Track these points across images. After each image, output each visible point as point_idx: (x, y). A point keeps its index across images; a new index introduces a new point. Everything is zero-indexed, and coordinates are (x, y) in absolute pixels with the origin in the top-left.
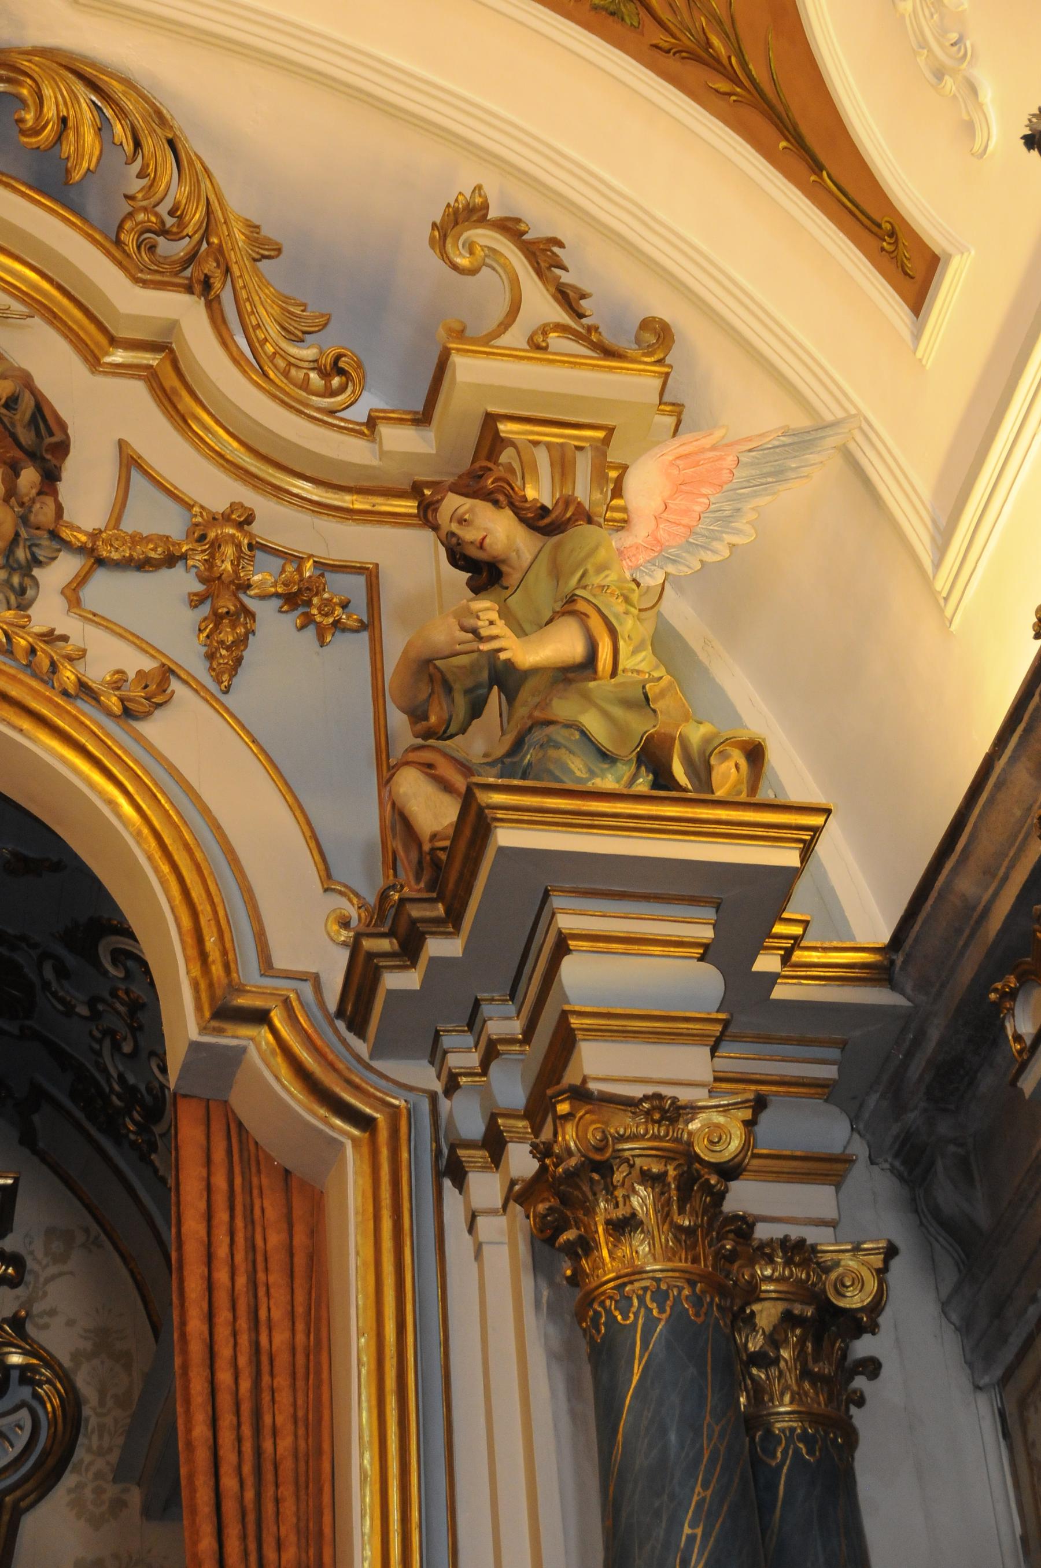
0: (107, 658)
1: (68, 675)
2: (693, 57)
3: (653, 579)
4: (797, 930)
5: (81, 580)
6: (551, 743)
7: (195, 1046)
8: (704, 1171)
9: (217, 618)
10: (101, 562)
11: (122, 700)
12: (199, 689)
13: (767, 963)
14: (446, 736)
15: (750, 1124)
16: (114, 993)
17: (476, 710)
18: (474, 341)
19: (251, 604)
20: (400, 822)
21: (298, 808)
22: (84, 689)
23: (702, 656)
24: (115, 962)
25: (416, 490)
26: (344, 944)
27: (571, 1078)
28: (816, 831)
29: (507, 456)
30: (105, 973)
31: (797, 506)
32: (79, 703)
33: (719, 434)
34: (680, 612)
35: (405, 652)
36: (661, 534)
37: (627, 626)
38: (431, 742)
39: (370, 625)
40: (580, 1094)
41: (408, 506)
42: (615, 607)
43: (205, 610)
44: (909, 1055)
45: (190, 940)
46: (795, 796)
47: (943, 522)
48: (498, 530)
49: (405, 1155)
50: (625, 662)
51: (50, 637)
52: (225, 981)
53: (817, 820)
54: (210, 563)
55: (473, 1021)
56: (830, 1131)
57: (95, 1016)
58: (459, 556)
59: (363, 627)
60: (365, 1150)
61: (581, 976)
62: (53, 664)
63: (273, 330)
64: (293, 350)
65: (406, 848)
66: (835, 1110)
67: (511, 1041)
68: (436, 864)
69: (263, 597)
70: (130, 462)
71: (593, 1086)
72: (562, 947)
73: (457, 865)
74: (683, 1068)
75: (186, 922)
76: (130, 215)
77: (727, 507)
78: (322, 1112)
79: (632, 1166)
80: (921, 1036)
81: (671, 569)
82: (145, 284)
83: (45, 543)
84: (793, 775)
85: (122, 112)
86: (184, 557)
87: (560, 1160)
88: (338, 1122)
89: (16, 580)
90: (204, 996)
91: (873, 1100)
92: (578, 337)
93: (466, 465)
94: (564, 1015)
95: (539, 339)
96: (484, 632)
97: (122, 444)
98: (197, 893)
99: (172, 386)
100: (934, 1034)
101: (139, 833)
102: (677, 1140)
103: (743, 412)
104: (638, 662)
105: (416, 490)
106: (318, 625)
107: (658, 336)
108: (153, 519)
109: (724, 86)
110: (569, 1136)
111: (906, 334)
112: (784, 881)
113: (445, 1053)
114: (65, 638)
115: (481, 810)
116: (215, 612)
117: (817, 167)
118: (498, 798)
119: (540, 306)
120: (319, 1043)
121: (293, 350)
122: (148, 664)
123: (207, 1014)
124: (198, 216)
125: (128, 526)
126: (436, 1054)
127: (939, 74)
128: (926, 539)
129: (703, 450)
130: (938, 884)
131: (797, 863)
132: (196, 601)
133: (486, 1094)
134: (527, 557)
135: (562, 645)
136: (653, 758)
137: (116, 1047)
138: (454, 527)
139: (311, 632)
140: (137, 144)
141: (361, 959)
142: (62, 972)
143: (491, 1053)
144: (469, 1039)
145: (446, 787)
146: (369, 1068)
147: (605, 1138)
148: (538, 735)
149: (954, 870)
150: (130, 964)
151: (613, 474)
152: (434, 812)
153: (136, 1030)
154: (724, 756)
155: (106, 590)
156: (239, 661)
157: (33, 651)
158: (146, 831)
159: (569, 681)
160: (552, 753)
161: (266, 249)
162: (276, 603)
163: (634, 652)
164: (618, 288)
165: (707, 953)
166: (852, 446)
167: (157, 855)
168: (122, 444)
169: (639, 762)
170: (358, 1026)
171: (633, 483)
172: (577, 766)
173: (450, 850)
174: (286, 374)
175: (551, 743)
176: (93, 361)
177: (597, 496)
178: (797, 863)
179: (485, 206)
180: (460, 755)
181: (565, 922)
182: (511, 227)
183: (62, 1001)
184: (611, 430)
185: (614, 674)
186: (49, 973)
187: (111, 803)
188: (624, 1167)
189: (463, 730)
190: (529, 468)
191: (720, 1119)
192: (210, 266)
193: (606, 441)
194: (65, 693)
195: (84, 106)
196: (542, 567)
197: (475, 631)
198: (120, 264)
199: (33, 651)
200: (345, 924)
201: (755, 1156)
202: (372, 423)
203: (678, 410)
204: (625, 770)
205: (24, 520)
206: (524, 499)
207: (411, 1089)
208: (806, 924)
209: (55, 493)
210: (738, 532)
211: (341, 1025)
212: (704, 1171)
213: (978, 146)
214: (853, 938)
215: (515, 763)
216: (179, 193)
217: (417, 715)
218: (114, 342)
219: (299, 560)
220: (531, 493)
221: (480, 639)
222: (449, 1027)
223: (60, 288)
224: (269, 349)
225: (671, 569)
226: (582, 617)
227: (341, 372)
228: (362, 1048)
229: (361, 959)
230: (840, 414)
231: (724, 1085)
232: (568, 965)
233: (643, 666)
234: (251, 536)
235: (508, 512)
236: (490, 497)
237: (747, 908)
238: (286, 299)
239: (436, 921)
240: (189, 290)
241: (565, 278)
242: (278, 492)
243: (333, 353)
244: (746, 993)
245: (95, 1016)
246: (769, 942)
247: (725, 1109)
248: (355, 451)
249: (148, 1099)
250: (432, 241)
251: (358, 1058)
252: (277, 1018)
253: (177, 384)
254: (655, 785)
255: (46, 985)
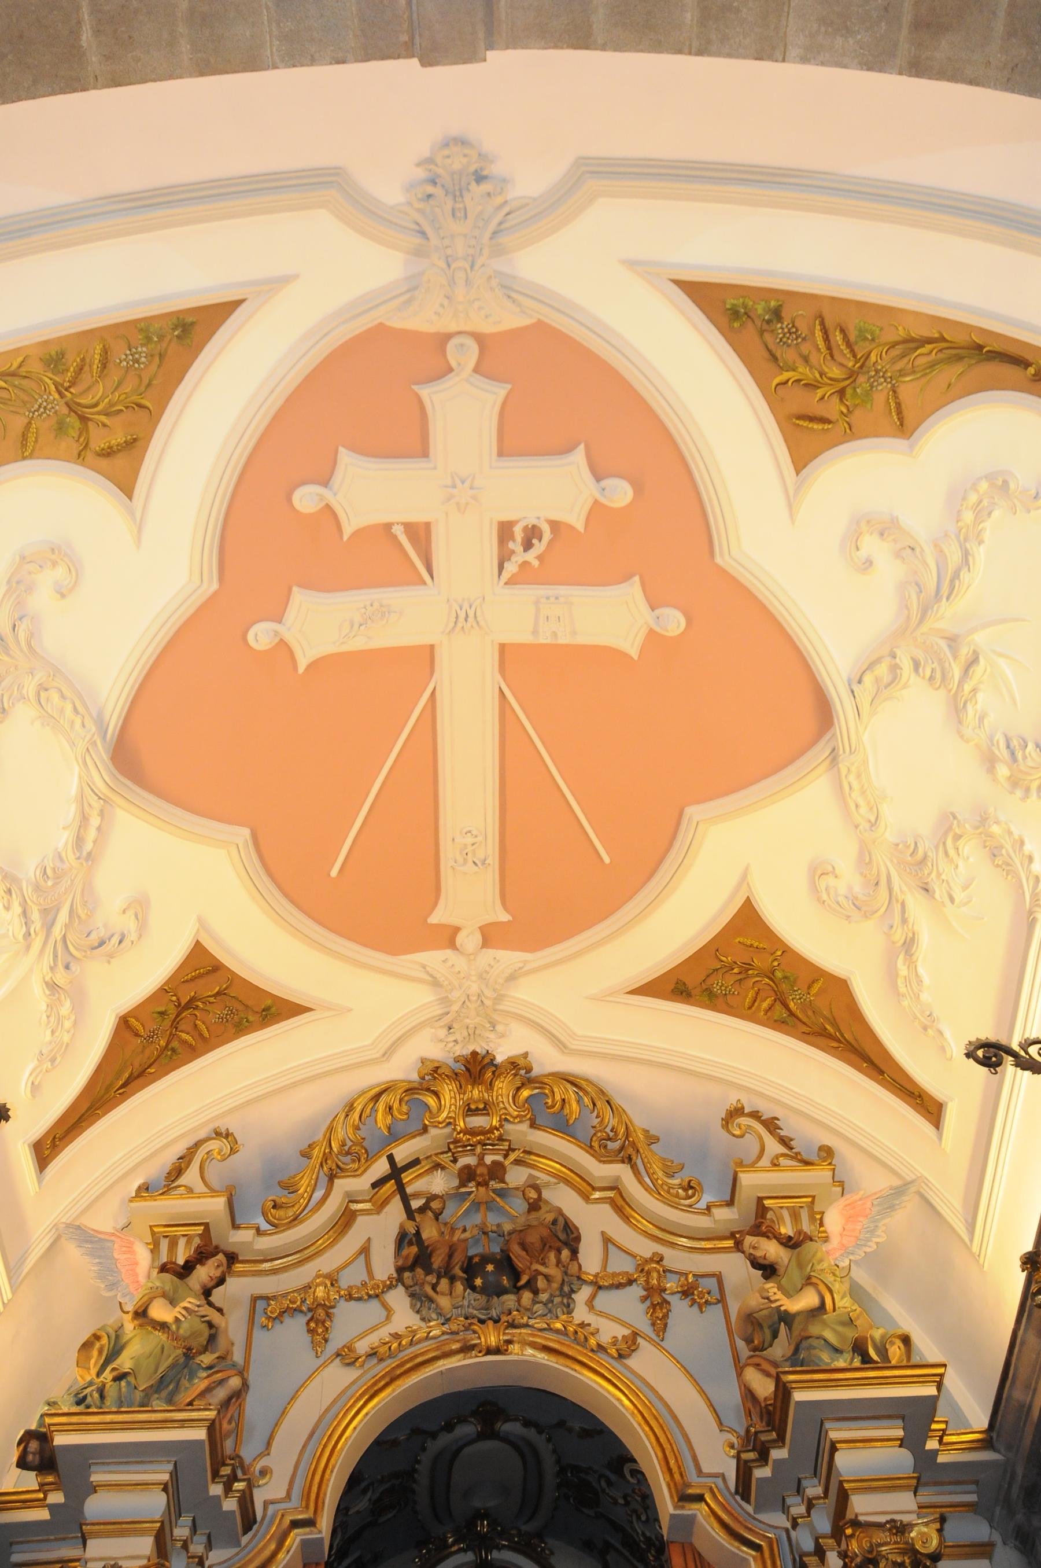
0: (609, 1332)
1: (592, 1342)
2: (820, 1035)
3: (845, 1263)
4: (943, 1426)
5: (593, 1297)
6: (811, 1347)
7: (672, 1516)
8: (923, 1559)
9: (654, 1306)
10: (600, 1287)
11: (617, 1350)
12: (650, 1340)
13: (932, 1444)
14: (763, 1349)
15: (940, 1531)
16: (634, 1491)
17: (775, 1335)
18: (747, 1166)
19: (668, 1298)
20: (749, 1394)
21: (702, 1392)
22: (601, 1348)
23: (874, 1295)
24: (632, 1476)
25: (732, 1236)
26: (733, 1457)
27: (849, 1516)
28: (942, 1375)
29: (770, 1215)
30: (628, 1482)
31: (905, 1216)
32: (599, 1354)
33: (862, 1192)
34: (860, 1275)
35: (739, 1312)
36: (844, 1242)
37: (836, 1287)
38: (757, 1353)
39: (722, 1300)
40: (855, 1523)
41: (730, 1243)
42: (829, 1279)
43: (648, 1303)
44: (1010, 1485)
45: (663, 1463)
46: (932, 1360)
47: (970, 1220)
48: (771, 1250)
49: (778, 1563)
50: (838, 1304)
51: (582, 1325)
52: (681, 1482)
53: (941, 1371)
54: (647, 1282)
55: (799, 1490)
56: (979, 1530)
57: (627, 1503)
58: (756, 1264)
59: (719, 1302)
60: (760, 1562)
61: (846, 1462)
62: (586, 1338)
63: (660, 1174)
64: (670, 1181)
65: (754, 1407)
66: (980, 1518)
67: (818, 1498)
68: (769, 1413)
69: (672, 1294)
70: (607, 1241)
71: (861, 1518)
72: (833, 1449)
73: (778, 1413)
74: (901, 1504)
75: (660, 1454)
76: (595, 1134)
77: (872, 1225)
78: (736, 1544)
79: (887, 1559)
80: (1013, 1477)
81: (851, 1257)
82: (604, 1162)
83: (575, 1282)
84: (927, 1349)
85: (586, 1093)
86: (635, 1280)
87: (852, 1560)
88: (745, 1549)
89: (565, 1301)
90: (673, 1490)
91: (998, 1510)
92: (792, 1158)
93: (752, 1222)
94: (841, 1482)
95: (775, 1161)
96: (772, 1299)
97: (603, 1233)
98: (663, 1440)
99: (620, 1204)
100: (1020, 1472)
101: (633, 1413)
102: (907, 1543)
103: (872, 1182)
104: (844, 1303)
105: (732, 1236)
106: (699, 1304)
107: (827, 1153)
108: (622, 1265)
109: (835, 1044)
110: (854, 1546)
111: (935, 1139)
112: (929, 1405)
113: (789, 1507)
114: (589, 1325)
115: (784, 1384)
116: (652, 1304)
117: (881, 1072)
118: (791, 1377)
119: (774, 1147)
120: (729, 1508)
121: (670, 1181)
122: (627, 1332)
123: (676, 1500)
124: (622, 1131)
125: (610, 1270)
126: (785, 1509)
127: (925, 1028)
128: (964, 1229)
129: (856, 1201)
130: (1005, 1396)
131: (935, 1393)
132: (644, 1299)
133: (812, 1527)
134: (786, 1261)
135: (807, 1300)
136: (859, 1348)
137: (639, 1518)
138: (751, 1251)
139: (696, 1307)
140: (594, 1105)
141: (742, 1462)
142: (610, 1483)
143: (810, 1506)
144: (799, 1499)
145: (768, 1375)
146: (755, 1519)
147: (871, 1545)
148: (804, 1344)
149: (1011, 1387)
150: (639, 1476)
151: (818, 1217)
152: (764, 1388)
153: (646, 1508)
154: (892, 1343)
155: (604, 1300)
156: (666, 1325)
157: (576, 1332)
158: (636, 1412)
159: (814, 1316)
160: (813, 1352)
161: (652, 1139)
162: (679, 1295)
163: (842, 1298)
164: (807, 1135)
165: (902, 1443)
166: (922, 1190)
167: (642, 1422)
168: (603, 1233)
169: (854, 1351)
170: (746, 1498)
171: (828, 1220)
172: (825, 1356)
173: (774, 1405)
174: (668, 1192)
175: (811, 1347)
176: (586, 1198)
177: (813, 1227)
178: (935, 1393)
179: (743, 1108)
180: (771, 1358)
181: (833, 1435)
182: (755, 1115)
183: (611, 1497)
184: (814, 1197)
185: (834, 1310)
186: (603, 1484)
187: (619, 1400)
188: (884, 1560)
189: (771, 1346)
190: (780, 1219)
191: (925, 1530)
192: (630, 1151)
193: (813, 1202)
194: (592, 1350)
195: (571, 1092)
196: (794, 1263)
197: (768, 1298)
198: (593, 1156)
199: (576, 1332)
200: (732, 1447)
201: (946, 1547)
202: (708, 1208)
203: (841, 1184)
204: (847, 1356)
205: (566, 1273)
206: (780, 1234)
207: (776, 1528)
208: (946, 1422)
209: (577, 1259)
210: (879, 1236)
211: (738, 1498)
212: (923, 1559)
213: (948, 1055)
214: (971, 1427)
215: (798, 1359)
216: (614, 1122)
217: (749, 1341)
218: (594, 1189)
219: (686, 1275)
220: (783, 1231)
221: (771, 1302)
222: (789, 1493)
223: (569, 1169)
224: (660, 1182)
225: (851, 1257)
226: (815, 1285)
227: (692, 1188)
228: (750, 1509)
229: (742, 1462)
230: (914, 1177)
231: (924, 1510)
232: (838, 1456)
233: (847, 1305)
234: (663, 1266)
235: (775, 1241)
236: (764, 1235)
237: (917, 1418)
238: (664, 1159)
239: (774, 1441)
240: (623, 1162)
241: (782, 1133)
242: (673, 1245)
243: (687, 1180)
244: (925, 1461)
245: (627, 1503)
246: (931, 1434)
247: (926, 1524)
248: (702, 1222)
249: (657, 1543)
250: (723, 1126)
251: (748, 1514)
252: (708, 1498)
253: (623, 1203)
254: (863, 1362)
255: (603, 1491)
